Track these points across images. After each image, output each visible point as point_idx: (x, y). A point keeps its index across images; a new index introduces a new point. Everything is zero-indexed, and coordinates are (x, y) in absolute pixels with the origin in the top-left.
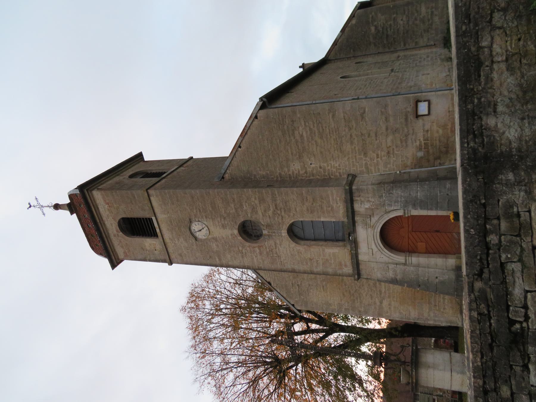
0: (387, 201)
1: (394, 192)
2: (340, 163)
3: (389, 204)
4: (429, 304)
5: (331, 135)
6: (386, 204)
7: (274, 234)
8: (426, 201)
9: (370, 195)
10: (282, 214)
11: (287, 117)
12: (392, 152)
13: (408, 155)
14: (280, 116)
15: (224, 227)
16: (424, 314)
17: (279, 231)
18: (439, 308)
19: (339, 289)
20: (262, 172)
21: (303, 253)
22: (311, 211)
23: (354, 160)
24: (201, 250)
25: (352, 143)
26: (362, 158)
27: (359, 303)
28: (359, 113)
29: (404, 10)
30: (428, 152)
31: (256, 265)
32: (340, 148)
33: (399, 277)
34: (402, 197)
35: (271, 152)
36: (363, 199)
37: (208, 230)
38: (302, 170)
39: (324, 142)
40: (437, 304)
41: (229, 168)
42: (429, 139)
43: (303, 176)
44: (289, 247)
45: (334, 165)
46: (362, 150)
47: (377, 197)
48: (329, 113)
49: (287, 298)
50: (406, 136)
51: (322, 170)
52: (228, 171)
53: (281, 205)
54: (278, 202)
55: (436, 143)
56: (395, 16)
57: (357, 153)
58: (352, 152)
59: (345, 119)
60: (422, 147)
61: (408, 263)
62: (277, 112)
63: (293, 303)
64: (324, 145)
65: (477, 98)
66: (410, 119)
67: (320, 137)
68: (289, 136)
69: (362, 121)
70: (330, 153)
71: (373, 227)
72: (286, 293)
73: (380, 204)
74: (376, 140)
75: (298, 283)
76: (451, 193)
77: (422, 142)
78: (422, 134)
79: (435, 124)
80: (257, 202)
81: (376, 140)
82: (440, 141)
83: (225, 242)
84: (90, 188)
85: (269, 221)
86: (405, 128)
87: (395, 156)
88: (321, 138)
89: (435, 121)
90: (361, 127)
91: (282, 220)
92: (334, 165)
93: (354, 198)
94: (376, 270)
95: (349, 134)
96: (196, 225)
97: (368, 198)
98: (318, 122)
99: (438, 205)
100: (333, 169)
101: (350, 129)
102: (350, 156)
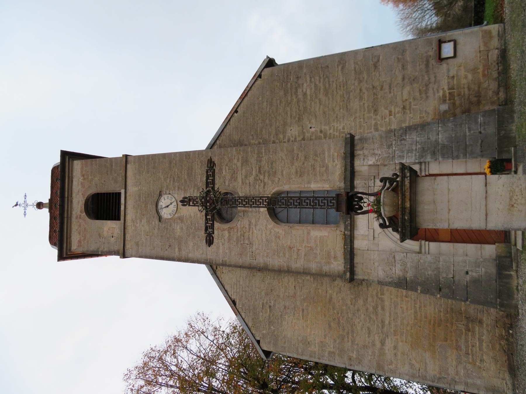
0: (398, 152)
1: (407, 137)
2: (344, 125)
3: (400, 156)
4: (457, 350)
6: (396, 157)
8: (451, 145)
9: (376, 146)
10: (265, 180)
11: (292, 74)
12: (408, 107)
13: (428, 109)
14: (285, 73)
16: (450, 369)
18: (473, 360)
19: (325, 316)
21: (281, 238)
22: (300, 173)
23: (362, 120)
24: (161, 236)
25: (361, 99)
26: (371, 117)
27: (350, 344)
28: (372, 63)
30: (454, 104)
31: (221, 257)
32: (347, 106)
33: (409, 275)
34: (418, 144)
35: (268, 115)
36: (366, 152)
37: (176, 206)
38: (299, 136)
39: (329, 99)
40: (470, 351)
41: (220, 138)
42: (455, 87)
44: (266, 228)
45: (337, 127)
46: (373, 107)
47: (385, 147)
48: (338, 66)
49: (252, 329)
50: (427, 85)
51: (322, 135)
52: (218, 142)
53: (266, 167)
54: (264, 162)
55: (464, 92)
57: (366, 111)
58: (360, 110)
59: (355, 70)
60: (446, 97)
61: (423, 250)
62: (283, 68)
63: (258, 339)
66: (431, 64)
67: (326, 94)
68: (292, 95)
69: (374, 72)
72: (253, 319)
73: (389, 156)
75: (270, 302)
76: (485, 129)
77: (446, 91)
78: (446, 81)
79: (462, 68)
80: (239, 164)
81: (390, 92)
82: (469, 89)
83: (191, 223)
85: (248, 191)
86: (426, 76)
87: (412, 111)
88: (326, 95)
89: (462, 64)
90: (373, 78)
91: (264, 188)
92: (337, 127)
93: (355, 152)
94: (376, 264)
96: (165, 200)
97: (373, 150)
98: (325, 76)
99: (467, 149)
100: (335, 133)
101: (360, 82)
102: (358, 115)
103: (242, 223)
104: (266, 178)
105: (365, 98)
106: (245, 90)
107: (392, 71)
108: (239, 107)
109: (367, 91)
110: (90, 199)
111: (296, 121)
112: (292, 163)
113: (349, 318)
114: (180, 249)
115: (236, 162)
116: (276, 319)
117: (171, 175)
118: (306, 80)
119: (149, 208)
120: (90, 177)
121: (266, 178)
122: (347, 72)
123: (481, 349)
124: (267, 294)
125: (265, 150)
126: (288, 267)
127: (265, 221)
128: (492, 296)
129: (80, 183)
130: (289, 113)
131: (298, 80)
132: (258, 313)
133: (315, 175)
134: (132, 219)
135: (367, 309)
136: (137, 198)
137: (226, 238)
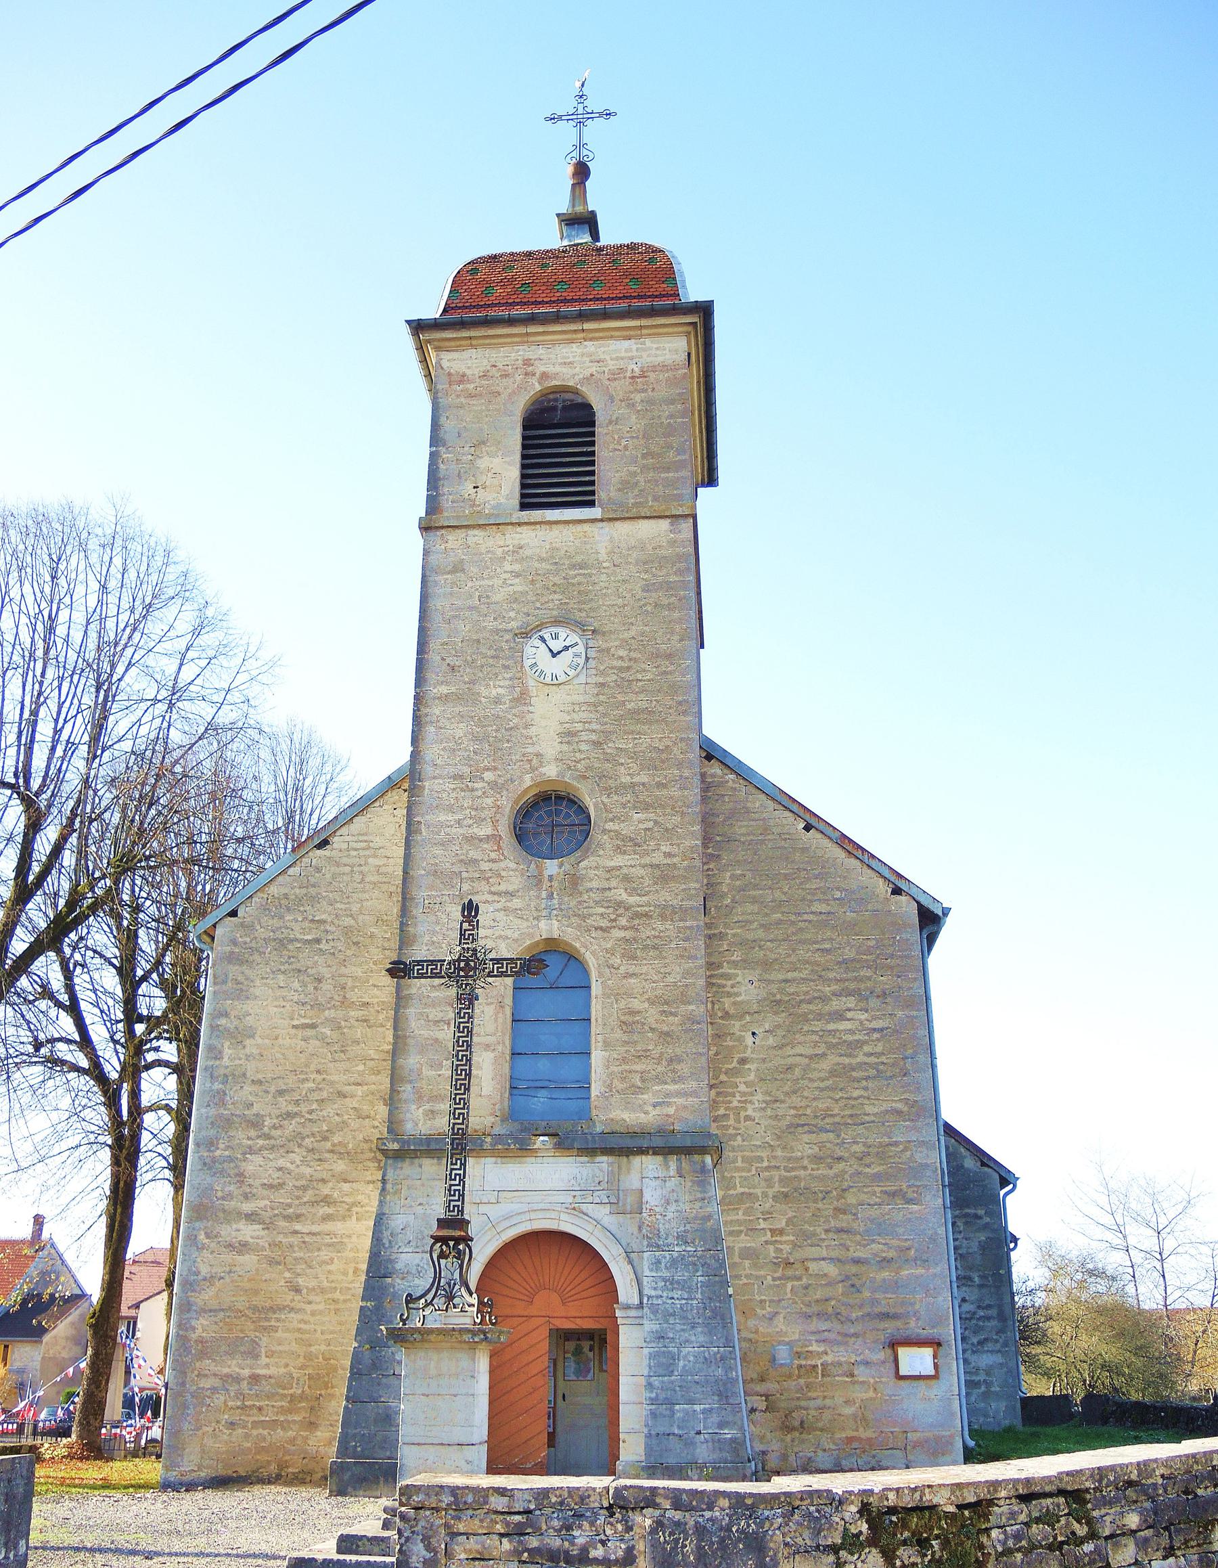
1: (700, 1279)
3: (659, 1262)
5: (841, 1103)
6: (657, 1253)
7: (544, 894)
8: (676, 1373)
12: (789, 1273)
15: (568, 736)
17: (555, 912)
20: (728, 881)
22: (630, 1024)
23: (765, 1164)
24: (478, 641)
25: (817, 1159)
29: (989, 1307)
31: (428, 817)
32: (803, 1125)
34: (684, 1302)
35: (793, 918)
37: (555, 682)
38: (734, 1003)
41: (741, 781)
43: (716, 1007)
44: (500, 937)
51: (735, 1064)
56: (976, 1279)
58: (789, 1159)
64: (811, 1080)
65: (9, 1558)
70: (787, 1094)
71: (575, 1210)
74: (827, 1231)
79: (871, 1394)
80: (657, 858)
84: (696, 336)
88: (833, 1073)
94: (419, 1210)
95: (846, 1155)
98: (881, 1067)
102: (779, 1153)
103: (511, 873)
104: (622, 934)
105: (818, 1169)
106: (863, 850)
107: (879, 1235)
108: (819, 836)
109: (836, 1176)
110: (580, 400)
111: (774, 995)
112: (652, 1002)
113: (303, 1139)
114: (445, 699)
115: (663, 848)
116: (289, 958)
117: (635, 660)
118: (874, 1018)
119: (551, 597)
120: (638, 397)
121: (622, 934)
122: (887, 1124)
123: (256, 1424)
124: (347, 931)
125: (690, 928)
126: (410, 997)
127: (516, 935)
128: (359, 1449)
129: (622, 364)
130: (795, 974)
131: (878, 997)
132: (302, 909)
133: (624, 1060)
134: (521, 548)
135: (323, 1181)
136: (579, 559)
137: (476, 830)
